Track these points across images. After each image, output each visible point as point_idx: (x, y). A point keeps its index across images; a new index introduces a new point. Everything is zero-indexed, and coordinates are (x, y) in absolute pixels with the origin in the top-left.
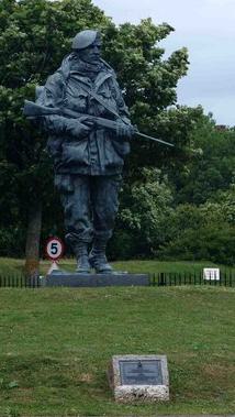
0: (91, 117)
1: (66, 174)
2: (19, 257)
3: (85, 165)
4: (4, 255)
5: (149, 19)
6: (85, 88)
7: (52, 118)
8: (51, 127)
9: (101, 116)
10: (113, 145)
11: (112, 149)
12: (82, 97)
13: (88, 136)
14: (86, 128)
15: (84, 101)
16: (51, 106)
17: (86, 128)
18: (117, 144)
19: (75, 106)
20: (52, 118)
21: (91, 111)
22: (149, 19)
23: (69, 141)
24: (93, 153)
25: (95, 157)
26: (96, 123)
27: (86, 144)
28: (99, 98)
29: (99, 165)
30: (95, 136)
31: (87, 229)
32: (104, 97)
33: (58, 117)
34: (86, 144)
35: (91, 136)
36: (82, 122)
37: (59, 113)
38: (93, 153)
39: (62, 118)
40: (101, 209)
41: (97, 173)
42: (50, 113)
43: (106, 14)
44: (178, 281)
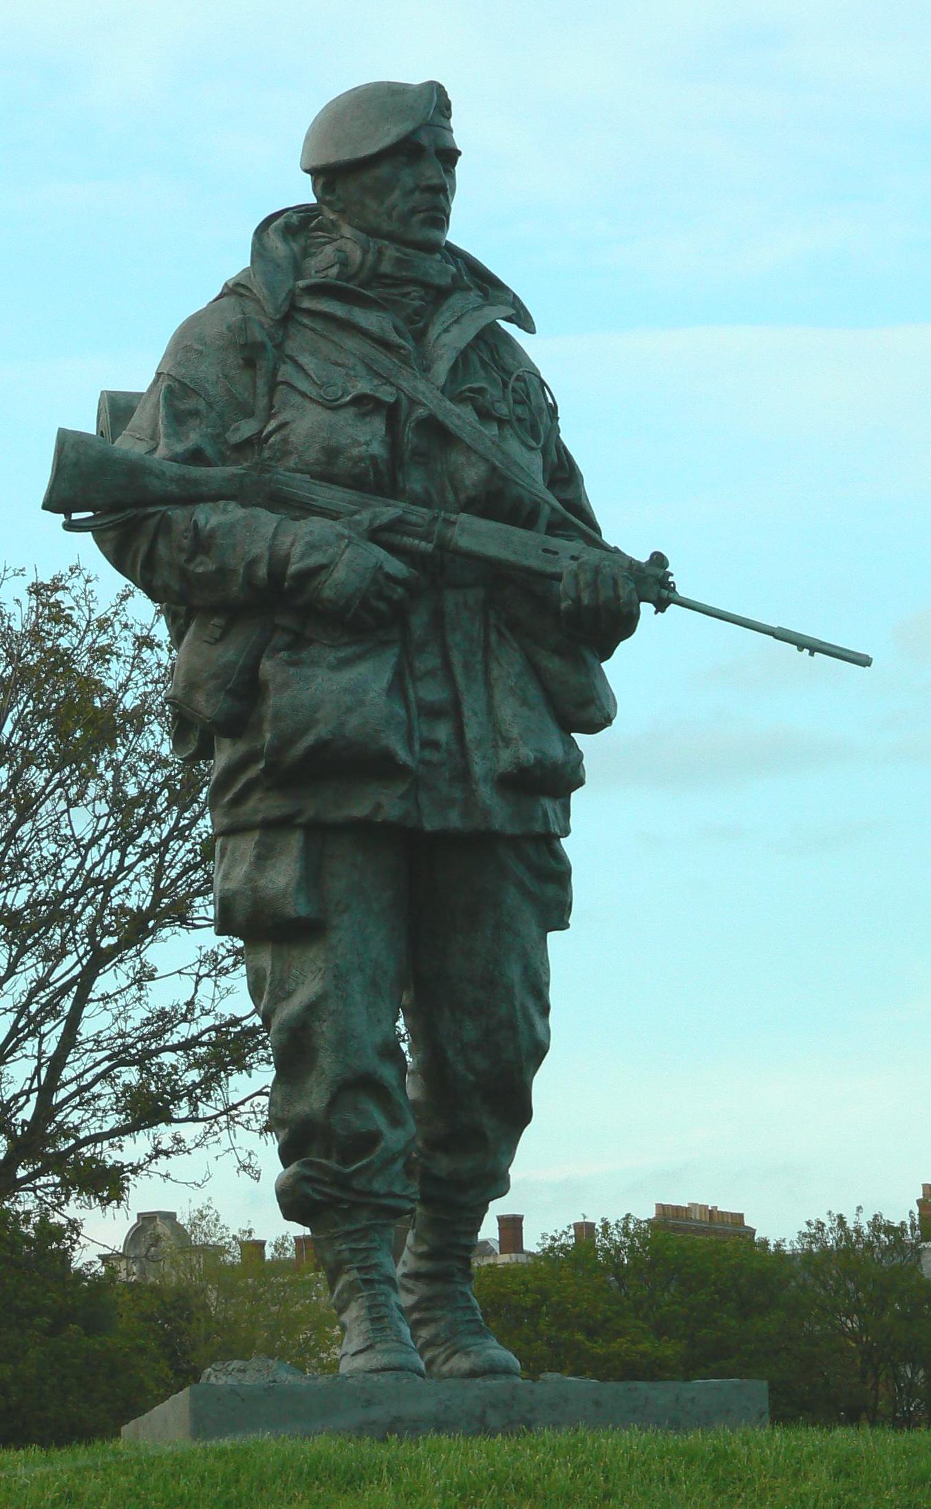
1: (276, 826)
4: (15, 1438)
6: (385, 361)
7: (209, 517)
9: (470, 506)
11: (533, 692)
13: (400, 614)
14: (395, 566)
15: (378, 425)
16: (196, 457)
17: (395, 566)
18: (553, 664)
20: (209, 517)
21: (416, 482)
22: (656, 613)
23: (298, 642)
24: (432, 713)
25: (442, 732)
26: (444, 546)
27: (390, 657)
28: (460, 418)
29: (464, 776)
30: (438, 620)
31: (394, 1138)
32: (485, 415)
33: (235, 512)
34: (390, 657)
35: (419, 621)
36: (376, 535)
38: (432, 713)
39: (267, 520)
40: (471, 1032)
41: (454, 820)
42: (192, 497)
44: (384, 1310)
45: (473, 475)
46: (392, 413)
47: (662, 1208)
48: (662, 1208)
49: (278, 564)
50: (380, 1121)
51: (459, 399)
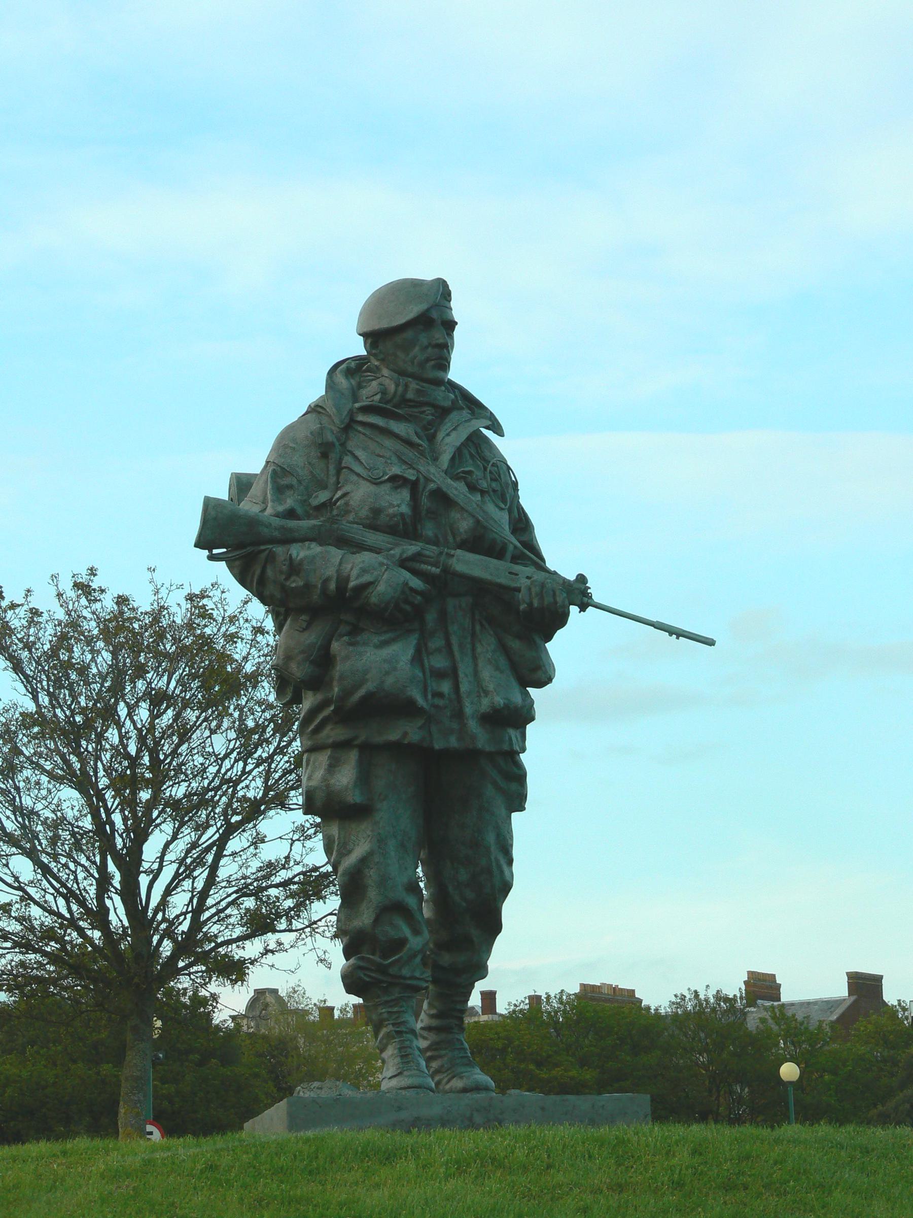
0: (431, 550)
2: (311, 731)
3: (408, 709)
5: (580, 612)
6: (409, 454)
7: (298, 552)
8: (296, 583)
10: (504, 648)
11: (503, 662)
12: (397, 481)
13: (419, 613)
14: (416, 583)
15: (405, 494)
16: (291, 514)
17: (416, 583)
19: (376, 512)
20: (298, 552)
21: (429, 530)
24: (439, 675)
25: (446, 687)
26: (446, 570)
27: (413, 640)
28: (457, 490)
29: (459, 714)
30: (443, 617)
32: (472, 488)
34: (413, 640)
35: (431, 617)
36: (404, 563)
37: (318, 537)
38: (439, 675)
39: (336, 554)
40: (463, 875)
41: (453, 742)
42: (288, 539)
43: (6, 1147)
45: (464, 525)
46: (414, 487)
47: (583, 986)
48: (583, 986)
49: (342, 581)
50: (406, 931)
51: (456, 478)
